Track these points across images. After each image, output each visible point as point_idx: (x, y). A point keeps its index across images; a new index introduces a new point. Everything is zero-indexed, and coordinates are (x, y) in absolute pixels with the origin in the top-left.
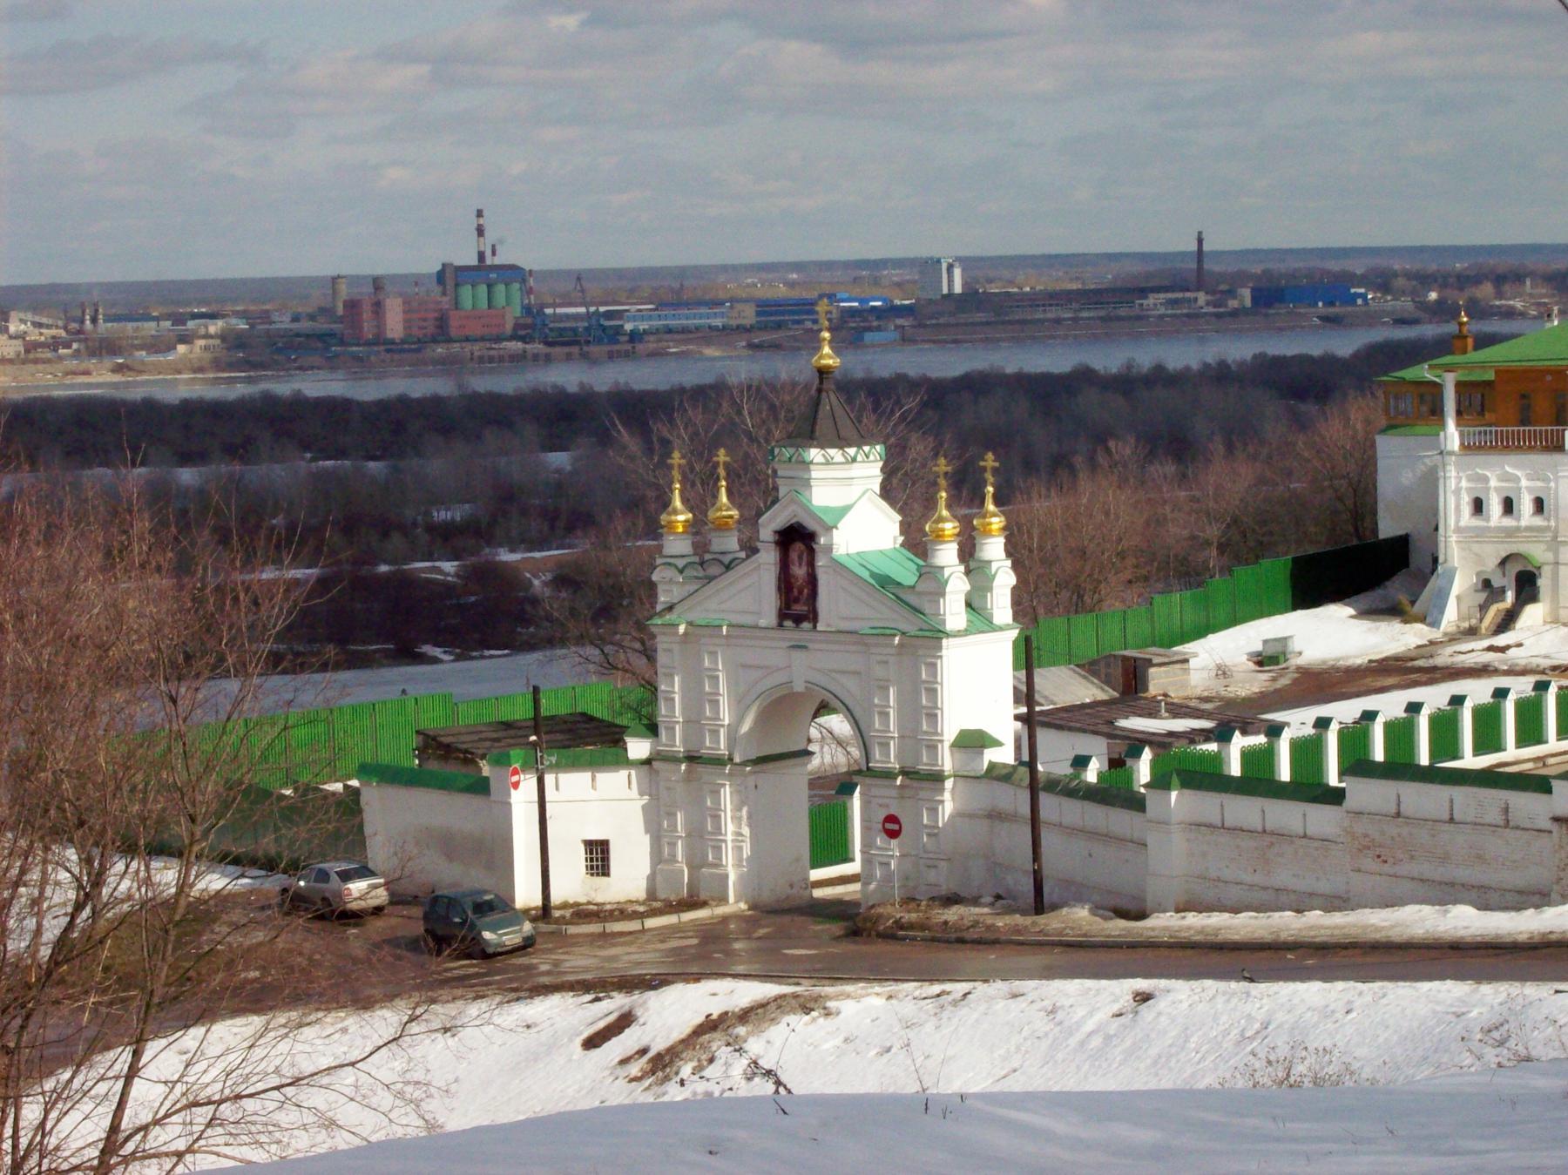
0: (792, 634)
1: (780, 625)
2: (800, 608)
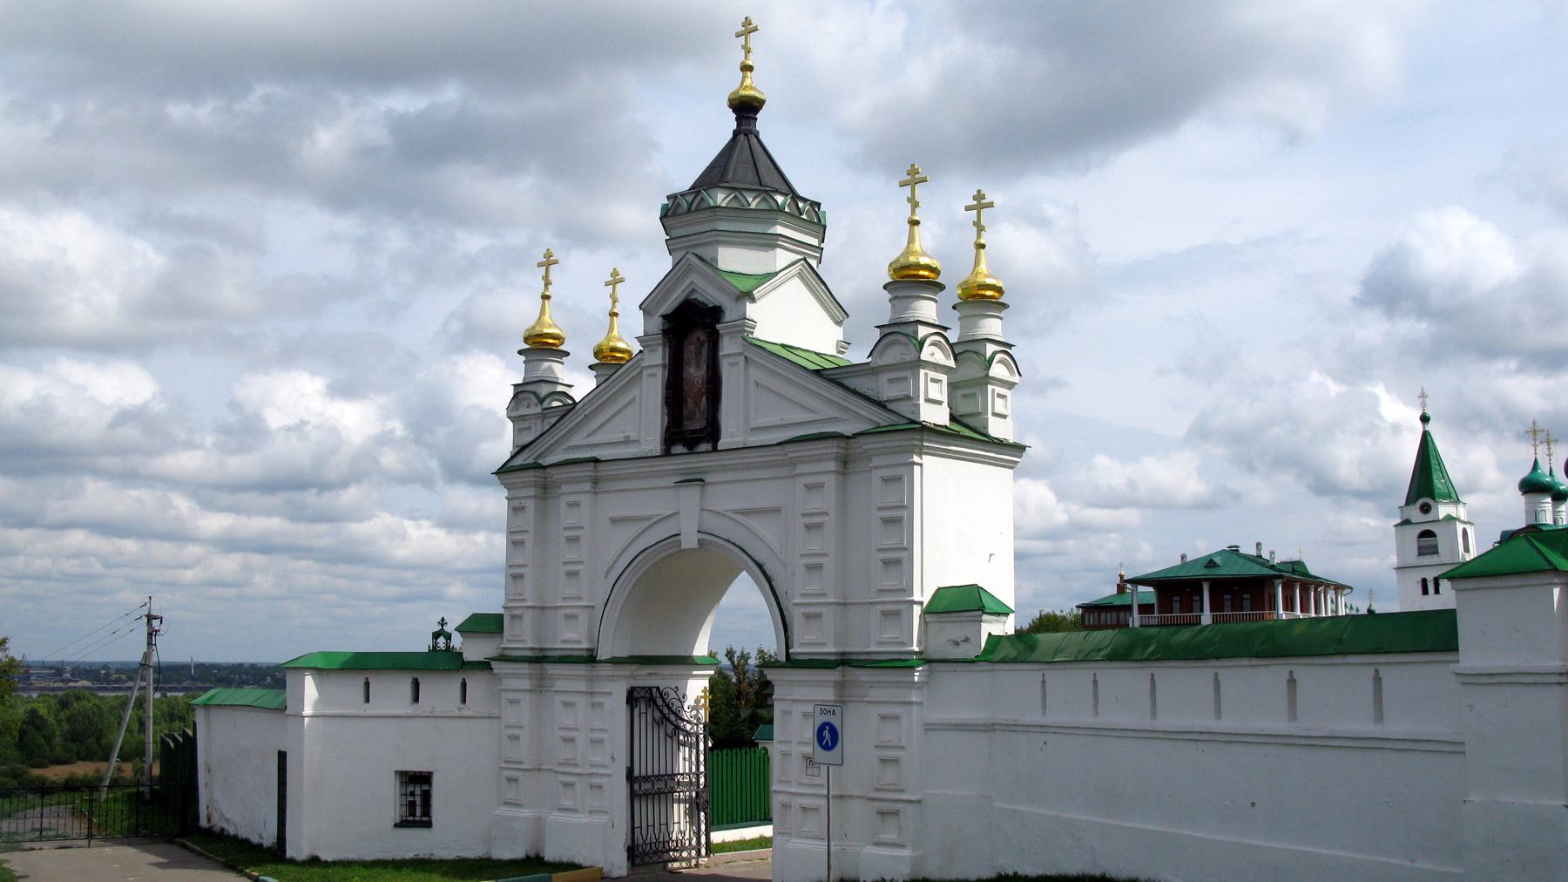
0: (685, 462)
1: (667, 453)
2: (697, 423)
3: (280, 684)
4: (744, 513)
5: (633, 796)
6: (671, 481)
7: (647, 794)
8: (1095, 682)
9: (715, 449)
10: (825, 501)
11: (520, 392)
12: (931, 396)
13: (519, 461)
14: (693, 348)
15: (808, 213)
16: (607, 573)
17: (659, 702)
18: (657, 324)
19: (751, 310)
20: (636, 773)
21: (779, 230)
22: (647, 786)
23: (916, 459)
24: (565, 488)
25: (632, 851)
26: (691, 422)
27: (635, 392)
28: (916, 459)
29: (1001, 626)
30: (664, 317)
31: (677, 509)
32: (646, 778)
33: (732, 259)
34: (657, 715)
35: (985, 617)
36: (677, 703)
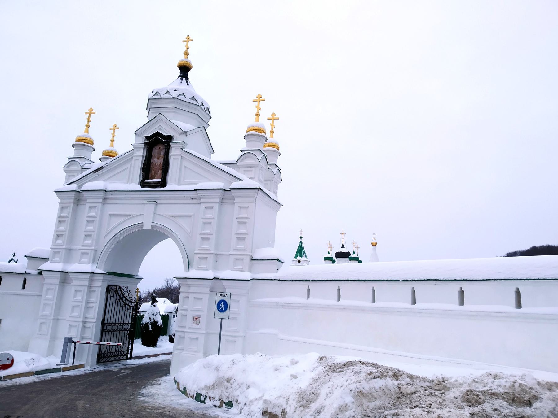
4: (170, 216)
5: (103, 331)
6: (141, 202)
8: (309, 290)
10: (212, 214)
11: (71, 161)
14: (157, 151)
16: (106, 236)
17: (120, 292)
18: (141, 141)
20: (106, 322)
22: (109, 328)
24: (89, 201)
27: (128, 166)
31: (142, 213)
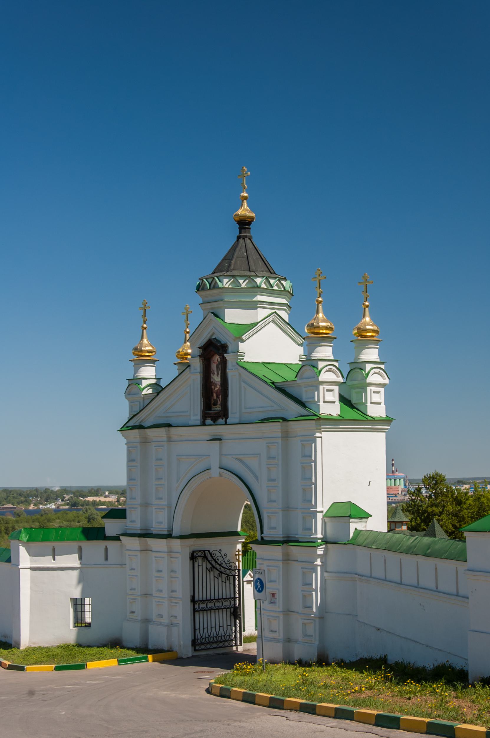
3: (224, 416)
5: (195, 611)
7: (203, 610)
9: (226, 423)
12: (327, 399)
13: (131, 423)
15: (277, 285)
17: (210, 558)
19: (242, 347)
20: (196, 598)
21: (259, 298)
22: (202, 606)
23: (318, 435)
25: (194, 643)
26: (214, 406)
28: (318, 435)
29: (363, 524)
30: (200, 348)
32: (203, 601)
33: (233, 316)
34: (209, 566)
35: (351, 520)
36: (221, 559)
